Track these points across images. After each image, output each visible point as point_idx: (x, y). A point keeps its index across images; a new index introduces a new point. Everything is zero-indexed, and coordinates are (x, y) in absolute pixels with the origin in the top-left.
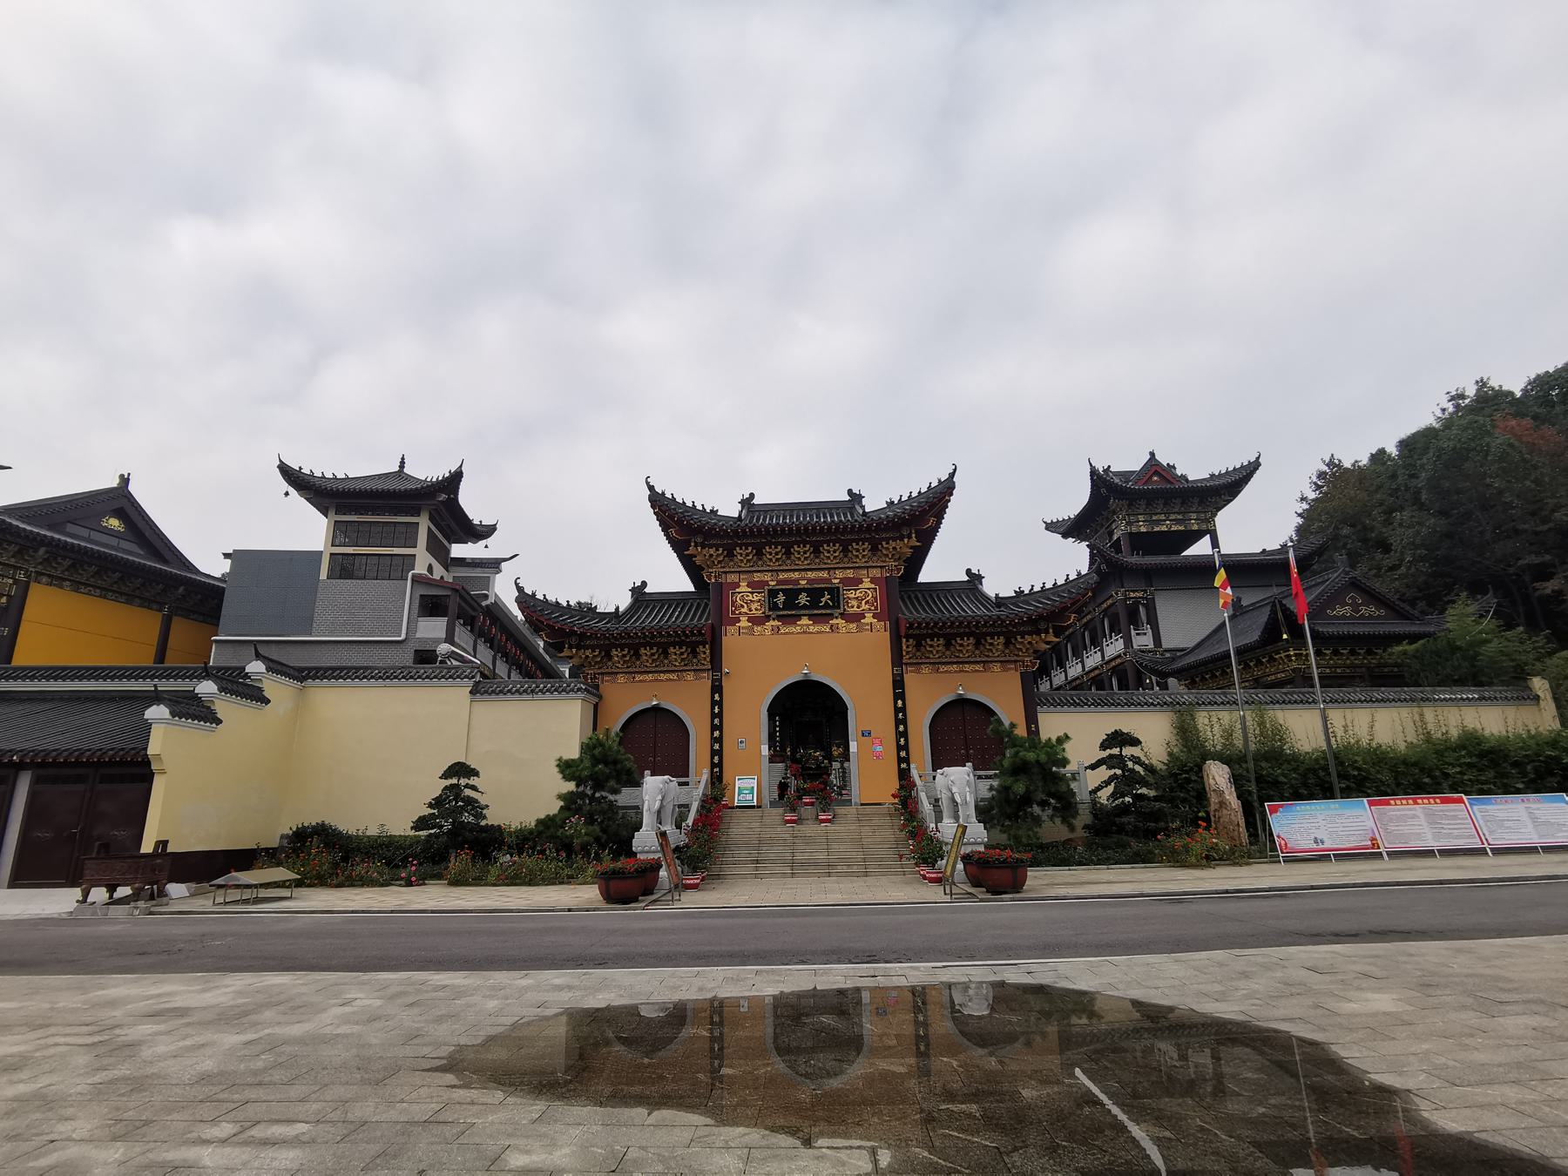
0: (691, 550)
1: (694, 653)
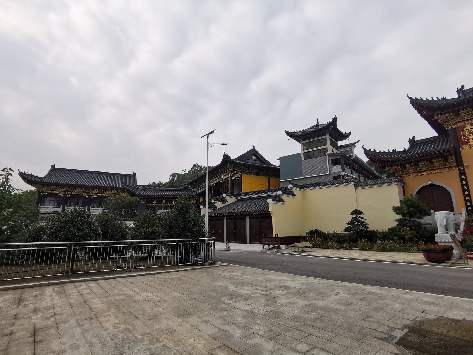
0: (435, 118)
1: (446, 160)
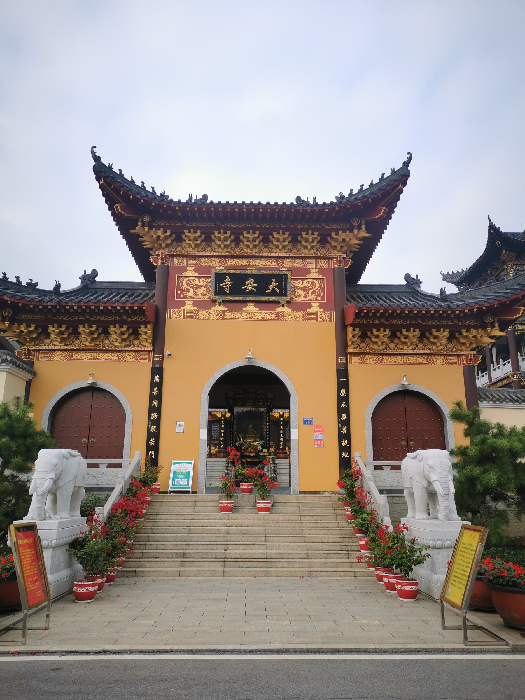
1: (136, 334)
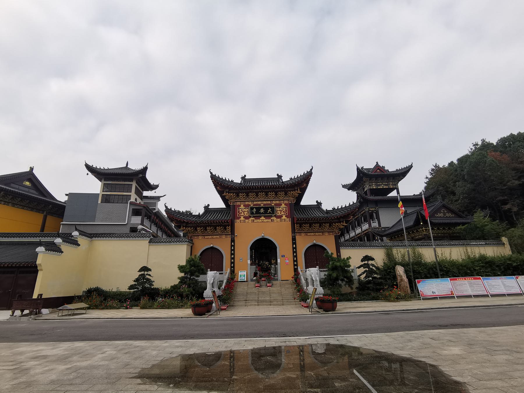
1: (225, 229)
